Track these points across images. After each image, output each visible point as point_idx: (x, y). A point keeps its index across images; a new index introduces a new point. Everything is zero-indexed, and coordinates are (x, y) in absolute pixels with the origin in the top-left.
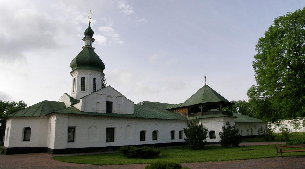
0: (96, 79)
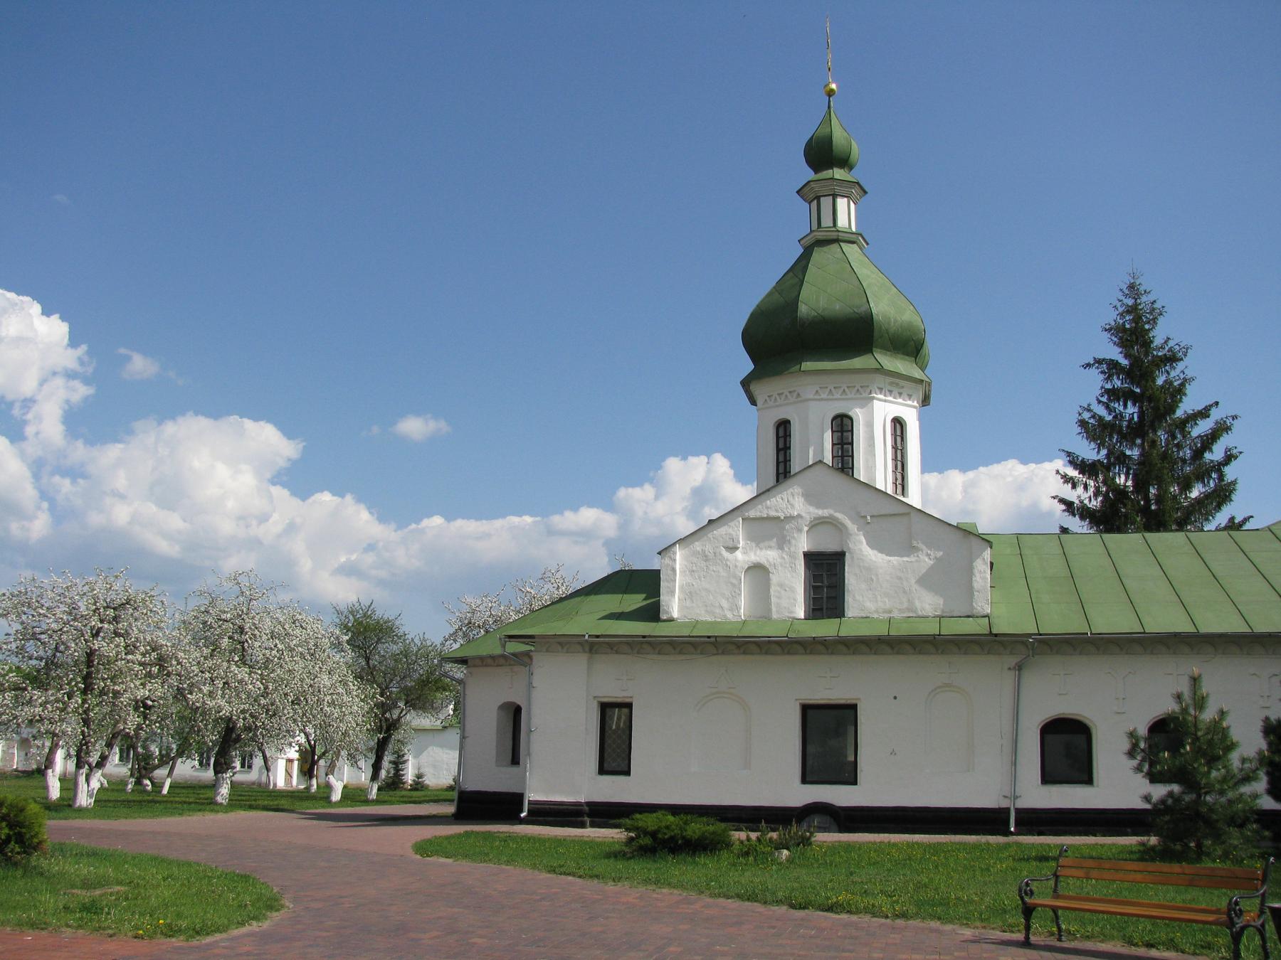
0: (851, 419)
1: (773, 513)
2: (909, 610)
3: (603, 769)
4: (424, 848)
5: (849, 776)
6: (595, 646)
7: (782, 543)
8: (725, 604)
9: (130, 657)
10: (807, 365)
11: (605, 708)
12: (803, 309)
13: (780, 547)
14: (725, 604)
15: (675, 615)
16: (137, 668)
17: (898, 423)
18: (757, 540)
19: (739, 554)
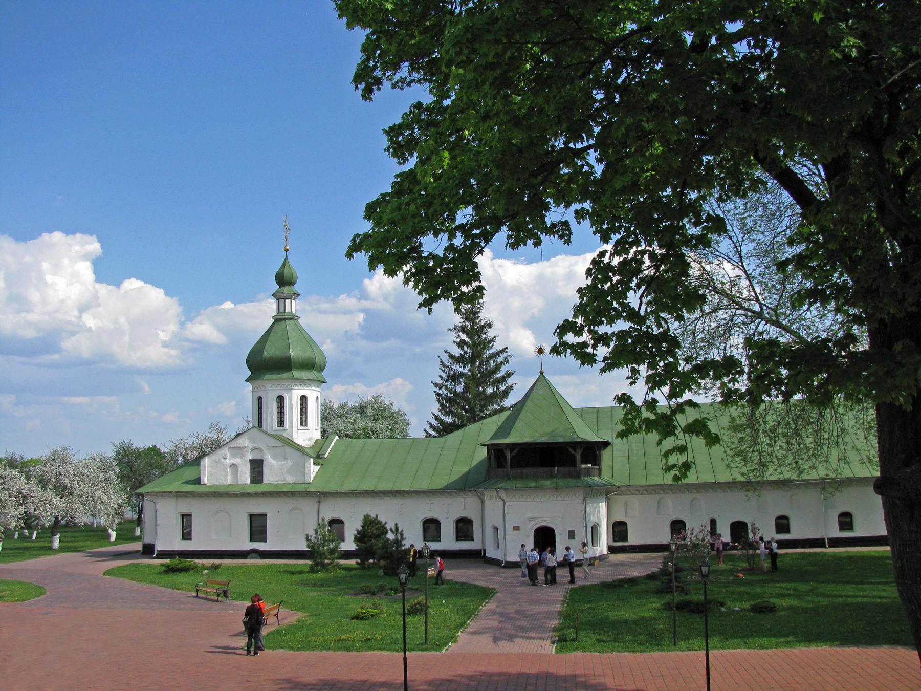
1: (239, 446)
2: (284, 481)
3: (183, 538)
4: (109, 572)
5: (264, 540)
6: (178, 495)
7: (242, 456)
8: (223, 479)
9: (11, 498)
10: (267, 377)
11: (183, 516)
12: (265, 354)
13: (241, 458)
14: (223, 479)
15: (206, 482)
16: (14, 503)
17: (304, 399)
18: (234, 455)
19: (227, 460)
